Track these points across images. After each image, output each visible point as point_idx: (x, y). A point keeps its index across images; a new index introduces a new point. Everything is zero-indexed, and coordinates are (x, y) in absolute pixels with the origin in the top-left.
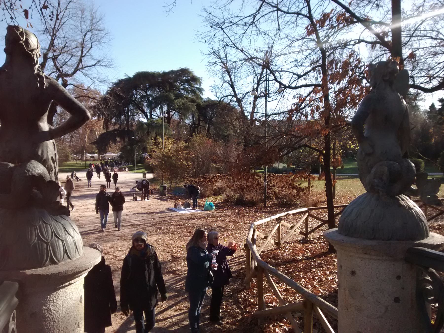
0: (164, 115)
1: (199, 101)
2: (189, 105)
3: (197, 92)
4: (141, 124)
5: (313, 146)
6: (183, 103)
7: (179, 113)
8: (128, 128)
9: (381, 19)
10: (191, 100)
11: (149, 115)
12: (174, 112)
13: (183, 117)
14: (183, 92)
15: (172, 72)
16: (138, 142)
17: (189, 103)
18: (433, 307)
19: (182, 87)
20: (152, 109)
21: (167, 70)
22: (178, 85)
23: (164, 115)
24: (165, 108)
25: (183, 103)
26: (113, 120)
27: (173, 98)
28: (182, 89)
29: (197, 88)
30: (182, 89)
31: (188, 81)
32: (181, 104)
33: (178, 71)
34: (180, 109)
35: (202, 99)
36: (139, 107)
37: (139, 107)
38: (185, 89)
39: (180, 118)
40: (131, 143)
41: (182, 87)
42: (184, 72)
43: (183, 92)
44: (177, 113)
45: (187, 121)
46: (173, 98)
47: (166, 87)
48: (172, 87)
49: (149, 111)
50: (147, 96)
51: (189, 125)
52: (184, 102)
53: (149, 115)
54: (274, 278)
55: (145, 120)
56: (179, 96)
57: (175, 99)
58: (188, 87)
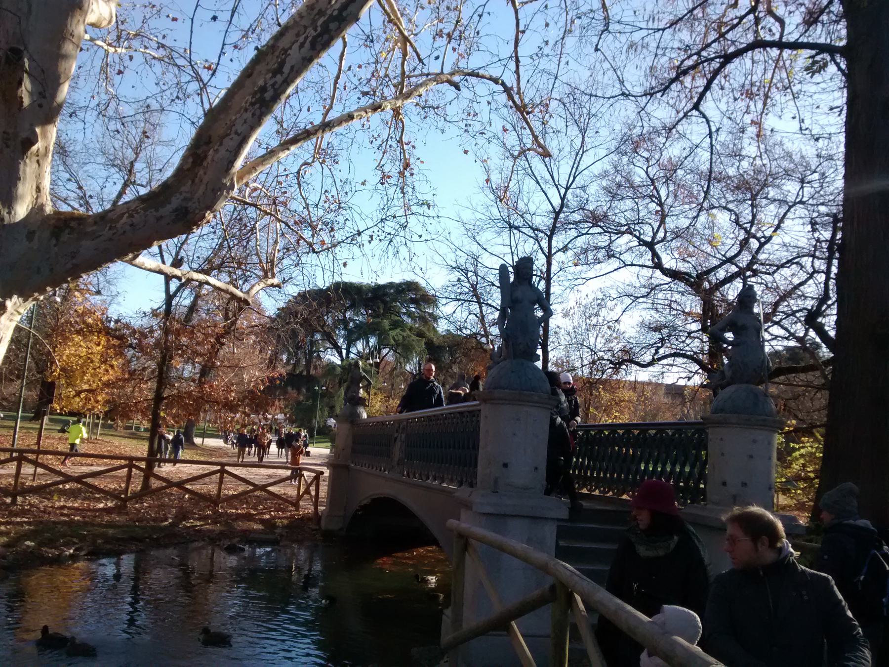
0: (375, 360)
1: (430, 335)
2: (413, 340)
3: (430, 320)
4: (331, 366)
5: (792, 38)
6: (403, 337)
7: (395, 351)
8: (308, 371)
9: (675, 381)
10: (418, 333)
11: (344, 352)
12: (388, 350)
13: (402, 360)
14: (405, 318)
15: (391, 285)
16: (323, 395)
17: (414, 337)
18: (111, 531)
19: (404, 310)
20: (350, 343)
21: (383, 281)
22: (397, 306)
23: (375, 360)
24: (373, 341)
25: (403, 337)
26: (285, 357)
27: (387, 328)
28: (404, 314)
29: (431, 315)
30: (404, 314)
31: (413, 301)
32: (401, 337)
33: (401, 284)
34: (398, 345)
35: (435, 330)
36: (329, 337)
37: (329, 337)
38: (410, 314)
39: (397, 360)
40: (313, 396)
41: (404, 310)
42: (410, 286)
43: (405, 318)
44: (392, 352)
45: (408, 368)
46: (387, 328)
47: (378, 308)
48: (389, 310)
49: (345, 346)
50: (345, 322)
51: (412, 373)
52: (405, 334)
53: (344, 352)
54: (492, 347)
55: (338, 362)
56: (396, 325)
57: (390, 329)
58: (414, 310)
